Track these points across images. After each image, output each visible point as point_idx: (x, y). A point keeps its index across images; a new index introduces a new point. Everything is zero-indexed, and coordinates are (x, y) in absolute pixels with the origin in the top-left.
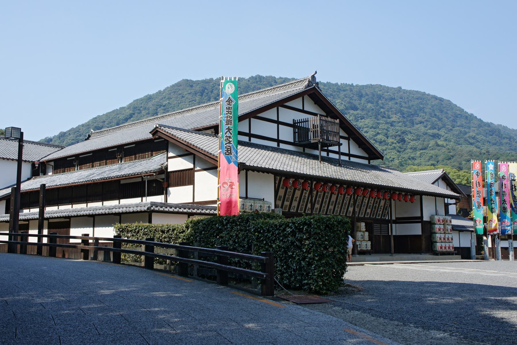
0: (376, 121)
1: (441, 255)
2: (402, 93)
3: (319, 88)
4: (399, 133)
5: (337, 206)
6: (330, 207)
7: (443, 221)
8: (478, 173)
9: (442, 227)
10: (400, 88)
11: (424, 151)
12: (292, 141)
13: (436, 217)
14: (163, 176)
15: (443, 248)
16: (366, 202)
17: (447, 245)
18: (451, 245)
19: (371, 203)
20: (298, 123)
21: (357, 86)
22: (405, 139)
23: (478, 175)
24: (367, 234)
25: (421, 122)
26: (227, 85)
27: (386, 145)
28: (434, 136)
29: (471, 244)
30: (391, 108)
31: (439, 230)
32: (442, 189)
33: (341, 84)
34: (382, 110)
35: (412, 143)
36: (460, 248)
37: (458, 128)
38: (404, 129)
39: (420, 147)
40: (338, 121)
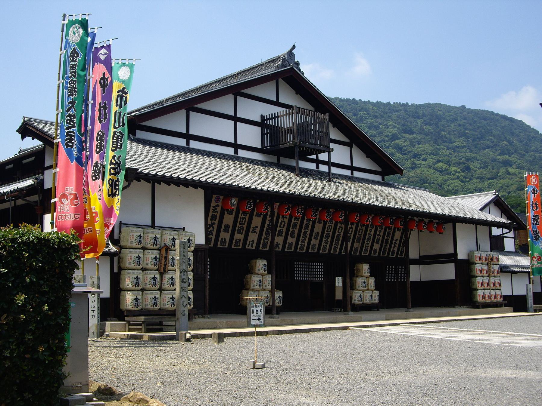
0: (436, 146)
1: (483, 308)
2: (465, 113)
3: (300, 70)
4: (463, 160)
5: (324, 240)
6: (313, 241)
7: (486, 259)
8: (534, 190)
9: (485, 267)
10: (464, 107)
11: (493, 181)
12: (259, 146)
13: (477, 254)
14: (34, 198)
15: (487, 298)
16: (372, 233)
17: (493, 293)
18: (498, 292)
19: (379, 235)
20: (267, 120)
21: (413, 105)
22: (471, 167)
23: (534, 193)
24: (372, 280)
25: (488, 147)
26: (71, 29)
27: (447, 174)
28: (507, 163)
29: (527, 290)
30: (454, 131)
31: (481, 272)
32: (495, 216)
33: (394, 103)
34: (443, 133)
35: (478, 171)
36: (512, 296)
37: (532, 153)
38: (469, 155)
39: (488, 176)
40: (327, 116)
